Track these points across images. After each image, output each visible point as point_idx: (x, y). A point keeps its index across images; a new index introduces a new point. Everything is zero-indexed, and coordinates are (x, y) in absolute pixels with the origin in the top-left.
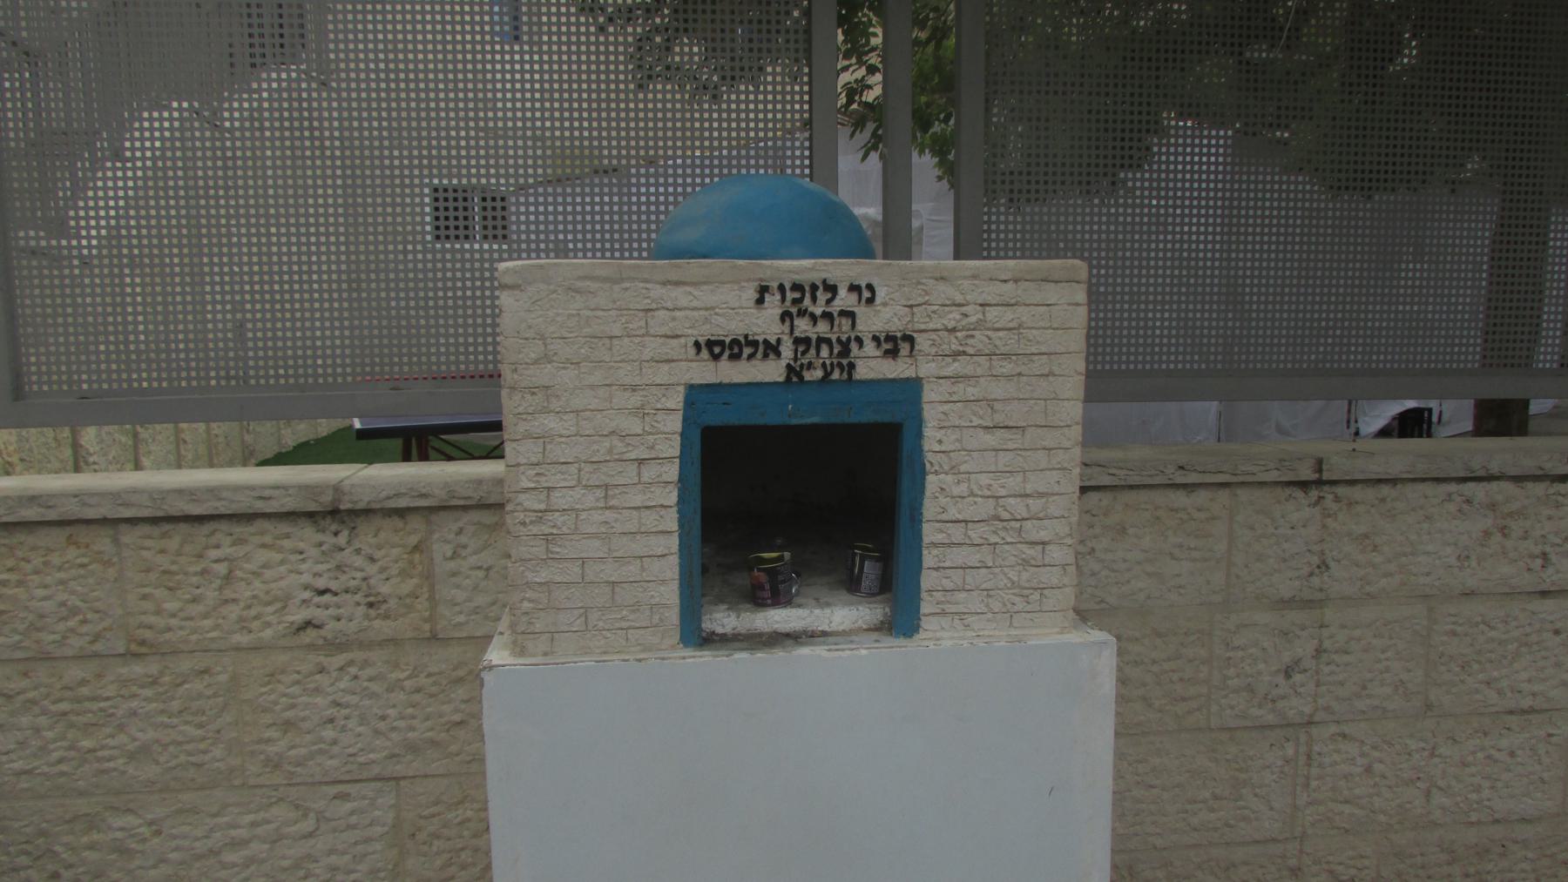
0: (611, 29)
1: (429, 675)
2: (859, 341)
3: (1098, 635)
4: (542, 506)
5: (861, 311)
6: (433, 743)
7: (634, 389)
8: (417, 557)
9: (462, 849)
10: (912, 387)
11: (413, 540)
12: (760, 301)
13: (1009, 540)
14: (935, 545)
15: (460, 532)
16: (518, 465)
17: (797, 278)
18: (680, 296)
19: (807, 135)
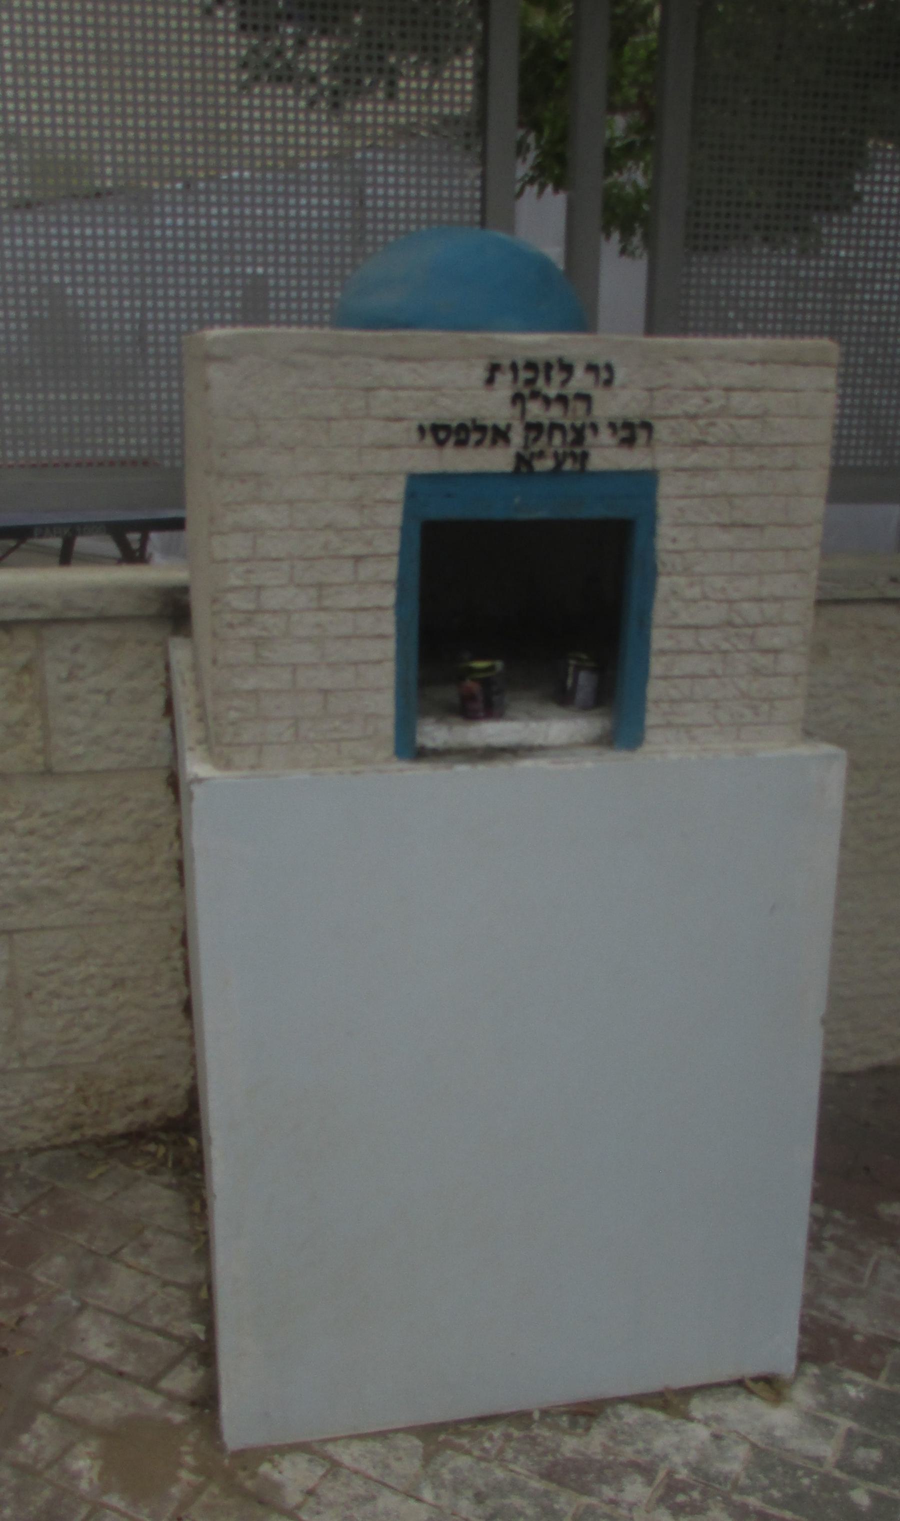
0: (220, 13)
1: (44, 815)
2: (594, 427)
3: (827, 749)
4: (251, 606)
5: (598, 395)
6: (51, 892)
7: (352, 477)
8: (26, 679)
9: (86, 1009)
10: (647, 481)
11: (21, 658)
12: (490, 381)
13: (741, 646)
14: (663, 652)
15: (75, 649)
16: (226, 561)
17: (533, 355)
18: (404, 373)
19: (478, 171)
